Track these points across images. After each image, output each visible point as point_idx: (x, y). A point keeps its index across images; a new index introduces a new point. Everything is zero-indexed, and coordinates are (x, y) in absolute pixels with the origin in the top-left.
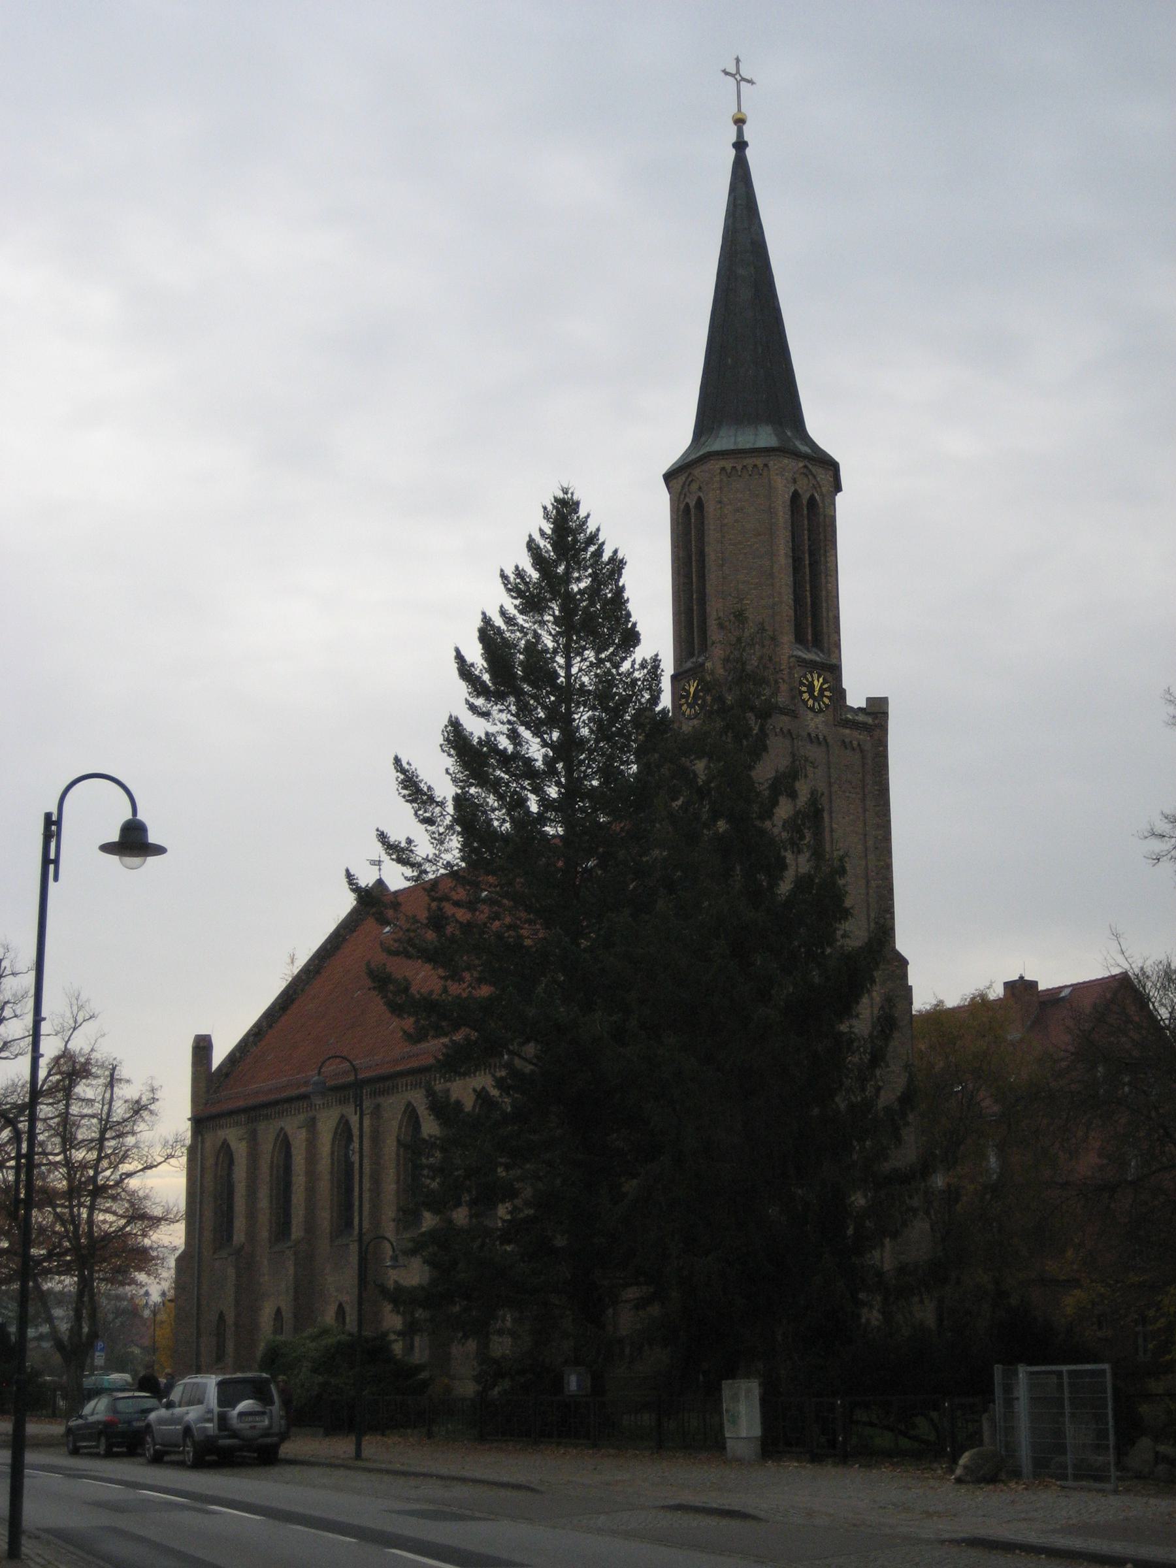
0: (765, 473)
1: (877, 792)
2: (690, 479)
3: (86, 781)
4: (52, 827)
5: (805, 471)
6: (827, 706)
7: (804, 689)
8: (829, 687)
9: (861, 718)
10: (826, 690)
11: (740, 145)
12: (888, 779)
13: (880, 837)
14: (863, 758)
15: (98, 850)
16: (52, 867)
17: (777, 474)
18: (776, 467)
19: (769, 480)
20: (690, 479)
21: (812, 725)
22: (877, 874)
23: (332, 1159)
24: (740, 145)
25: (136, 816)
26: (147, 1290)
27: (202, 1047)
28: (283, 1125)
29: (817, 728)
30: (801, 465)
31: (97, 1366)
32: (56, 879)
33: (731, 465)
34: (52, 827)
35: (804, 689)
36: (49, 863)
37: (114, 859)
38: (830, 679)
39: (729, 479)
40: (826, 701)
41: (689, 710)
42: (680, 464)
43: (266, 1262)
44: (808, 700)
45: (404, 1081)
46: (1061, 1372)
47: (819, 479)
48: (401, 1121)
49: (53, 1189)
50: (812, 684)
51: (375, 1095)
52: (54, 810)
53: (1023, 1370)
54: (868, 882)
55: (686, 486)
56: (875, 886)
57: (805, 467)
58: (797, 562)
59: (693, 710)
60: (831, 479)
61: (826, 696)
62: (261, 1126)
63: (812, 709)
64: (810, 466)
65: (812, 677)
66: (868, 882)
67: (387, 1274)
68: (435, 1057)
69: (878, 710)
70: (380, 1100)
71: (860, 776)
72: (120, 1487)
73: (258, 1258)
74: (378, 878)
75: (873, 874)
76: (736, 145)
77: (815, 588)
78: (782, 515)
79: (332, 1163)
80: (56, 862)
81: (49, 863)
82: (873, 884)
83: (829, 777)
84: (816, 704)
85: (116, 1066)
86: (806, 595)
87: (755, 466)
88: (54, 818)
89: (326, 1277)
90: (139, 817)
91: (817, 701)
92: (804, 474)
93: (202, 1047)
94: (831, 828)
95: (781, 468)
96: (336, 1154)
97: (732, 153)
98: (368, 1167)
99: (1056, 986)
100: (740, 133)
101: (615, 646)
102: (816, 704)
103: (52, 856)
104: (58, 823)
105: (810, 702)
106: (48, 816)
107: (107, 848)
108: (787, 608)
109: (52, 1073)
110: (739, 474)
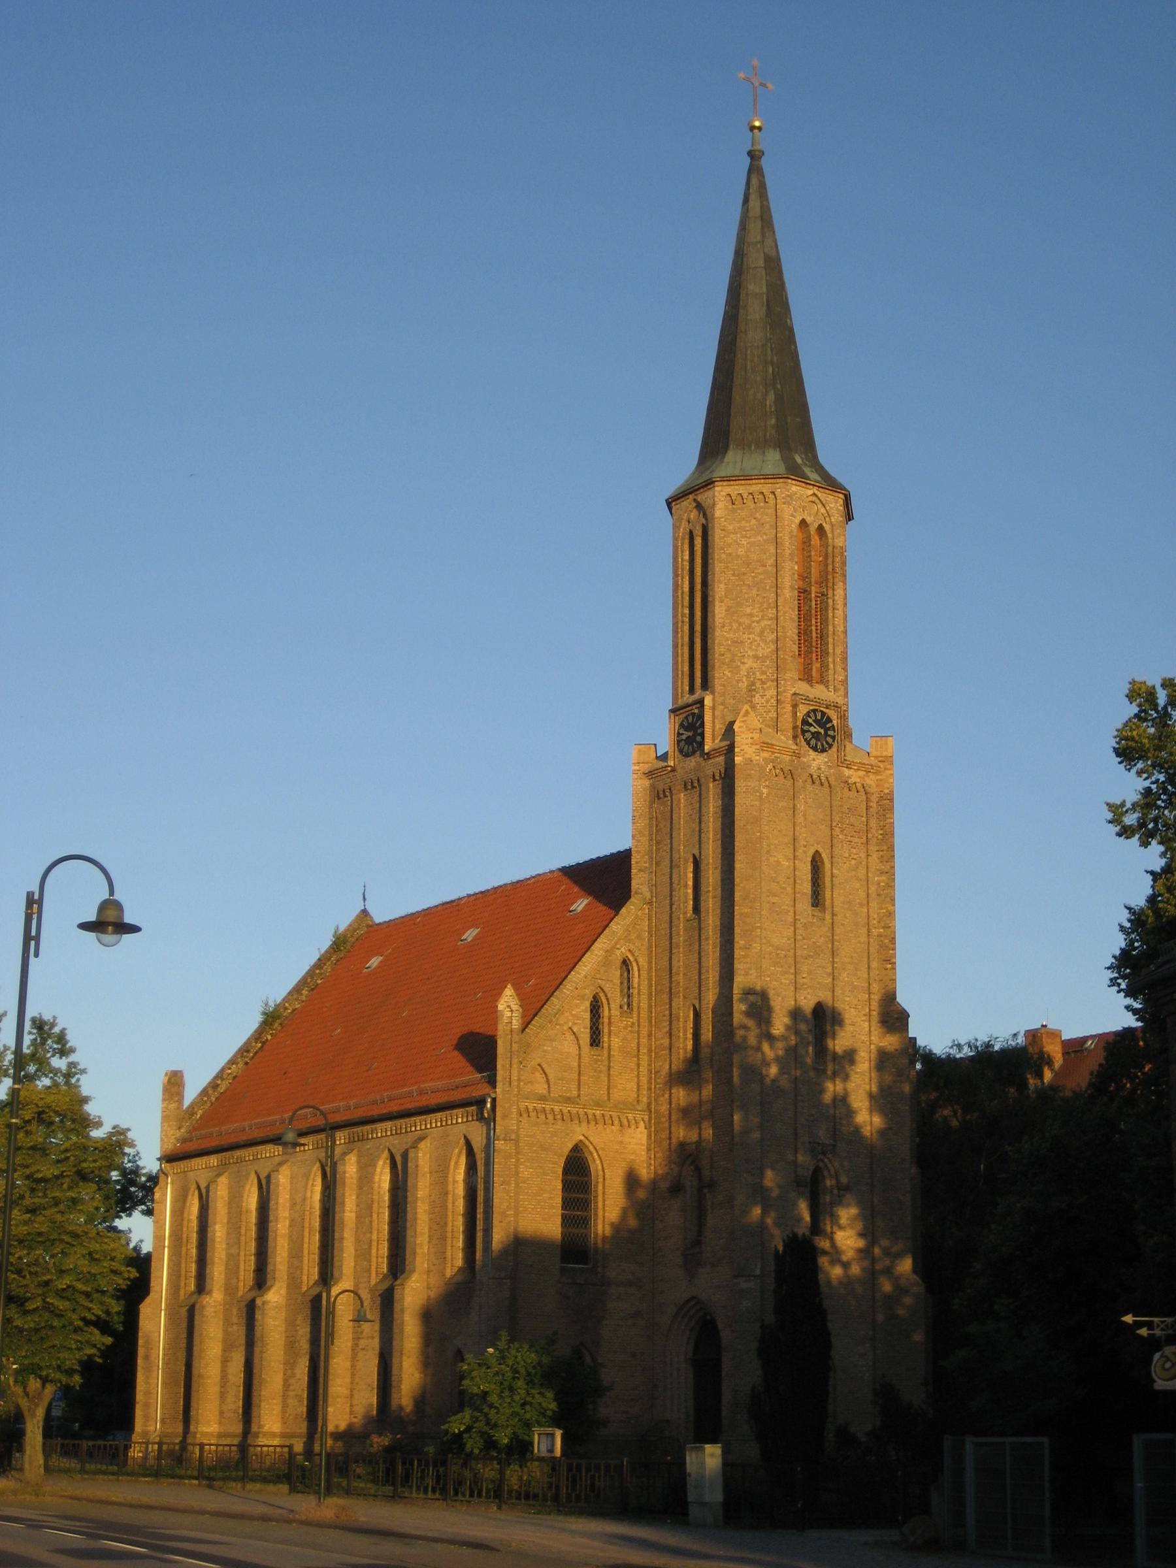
1: (880, 837)
4: (34, 904)
5: (814, 498)
13: (882, 884)
14: (868, 800)
15: (78, 929)
16: (33, 943)
17: (784, 503)
18: (784, 495)
21: (814, 765)
22: (879, 922)
25: (113, 896)
26: (34, 1020)
27: (174, 1083)
29: (819, 769)
30: (810, 492)
31: (1122, 821)
32: (37, 955)
34: (34, 904)
36: (31, 940)
37: (91, 936)
41: (686, 747)
42: (683, 489)
44: (811, 739)
47: (828, 508)
52: (35, 889)
53: (970, 1442)
56: (876, 934)
57: (814, 494)
59: (690, 747)
60: (842, 508)
61: (829, 735)
64: (819, 495)
71: (864, 819)
74: (363, 908)
75: (875, 922)
76: (751, 154)
78: (789, 545)
80: (37, 939)
81: (31, 940)
82: (874, 932)
84: (819, 744)
86: (811, 630)
88: (36, 897)
89: (298, 1328)
90: (117, 896)
91: (819, 740)
92: (813, 502)
93: (174, 1083)
94: (832, 873)
95: (788, 496)
99: (1081, 1035)
102: (819, 744)
103: (33, 933)
104: (40, 902)
106: (30, 896)
107: (85, 926)
108: (791, 643)
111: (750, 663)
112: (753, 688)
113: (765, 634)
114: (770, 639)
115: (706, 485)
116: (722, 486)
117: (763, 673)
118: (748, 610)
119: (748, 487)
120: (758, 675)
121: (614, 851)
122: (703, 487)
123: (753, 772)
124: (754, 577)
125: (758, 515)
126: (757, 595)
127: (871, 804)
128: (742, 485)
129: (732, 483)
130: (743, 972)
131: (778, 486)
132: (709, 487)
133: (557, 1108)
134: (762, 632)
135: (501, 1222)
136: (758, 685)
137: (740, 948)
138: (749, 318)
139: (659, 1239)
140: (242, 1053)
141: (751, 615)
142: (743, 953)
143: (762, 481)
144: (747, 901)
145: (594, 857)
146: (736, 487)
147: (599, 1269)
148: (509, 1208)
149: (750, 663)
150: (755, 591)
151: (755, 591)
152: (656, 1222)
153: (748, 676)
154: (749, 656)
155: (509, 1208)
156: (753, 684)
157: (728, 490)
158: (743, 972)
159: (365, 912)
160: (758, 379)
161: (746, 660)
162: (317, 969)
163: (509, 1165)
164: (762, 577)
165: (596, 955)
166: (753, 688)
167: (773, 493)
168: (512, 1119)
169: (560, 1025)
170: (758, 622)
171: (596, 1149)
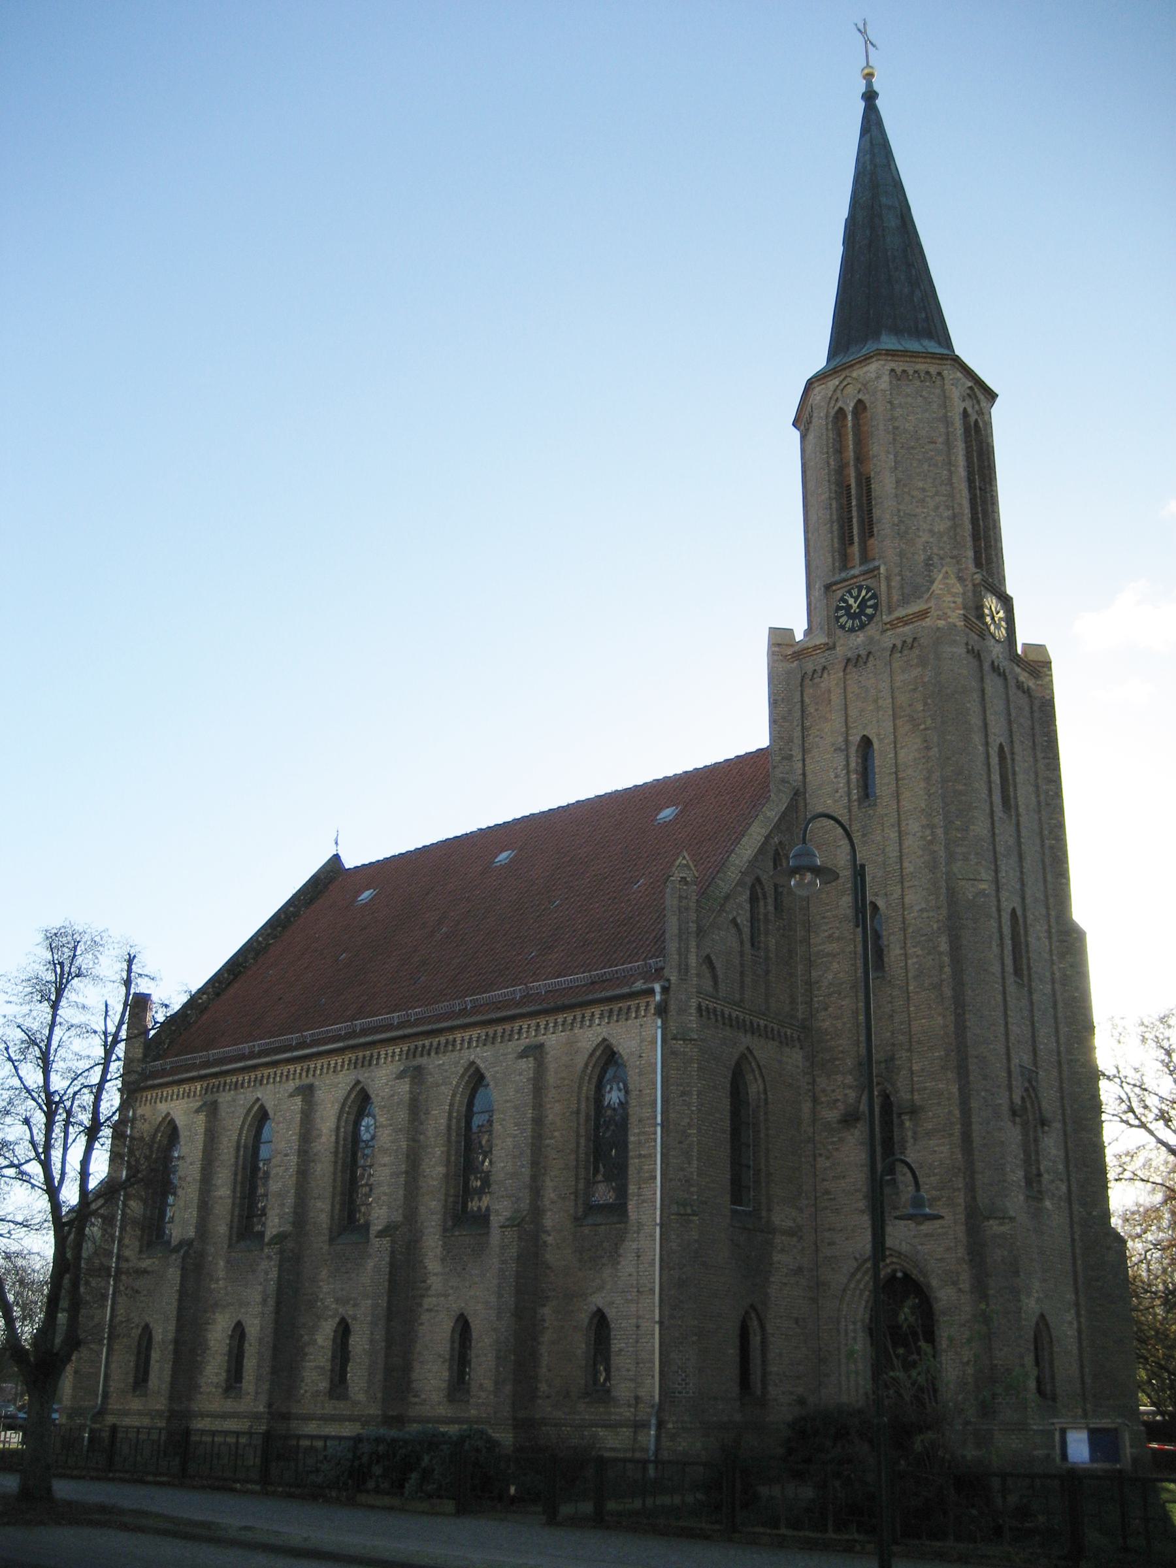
0: (938, 383)
2: (845, 383)
11: (870, 97)
12: (1055, 731)
13: (1051, 793)
17: (952, 385)
18: (951, 377)
19: (944, 391)
20: (845, 383)
23: (337, 1136)
24: (870, 97)
28: (259, 1095)
30: (970, 384)
33: (901, 369)
39: (899, 382)
43: (222, 1263)
45: (467, 1035)
48: (457, 1086)
51: (437, 1053)
54: (1042, 841)
55: (839, 392)
58: (970, 481)
62: (225, 1098)
66: (1042, 841)
67: (424, 1282)
68: (197, 1111)
70: (423, 1061)
73: (210, 1259)
77: (986, 513)
79: (337, 1142)
83: (1010, 715)
85: (135, 956)
87: (928, 373)
89: (321, 1284)
96: (342, 1130)
97: (861, 105)
98: (405, 1143)
100: (869, 84)
110: (911, 377)
111: (925, 537)
112: (931, 562)
113: (940, 510)
114: (946, 514)
115: (866, 359)
116: (886, 360)
117: (942, 548)
118: (920, 484)
119: (913, 364)
120: (935, 550)
121: (690, 768)
122: (860, 362)
123: (958, 638)
124: (924, 453)
125: (924, 393)
126: (929, 471)
127: (247, 1051)
128: (907, 362)
129: (896, 358)
130: (961, 857)
131: (944, 367)
132: (868, 362)
133: (727, 1012)
134: (937, 508)
135: (680, 1142)
136: (936, 559)
137: (957, 829)
138: (885, 225)
139: (824, 1180)
140: (214, 984)
141: (924, 490)
142: (959, 835)
143: (928, 360)
144: (960, 777)
145: (660, 777)
146: (901, 363)
147: (764, 1214)
148: (690, 1126)
149: (925, 537)
150: (926, 466)
151: (926, 466)
152: (819, 1159)
153: (925, 550)
154: (924, 530)
155: (690, 1126)
156: (930, 558)
157: (893, 365)
158: (961, 857)
159: (336, 858)
160: (902, 277)
161: (921, 534)
162: (291, 906)
163: (690, 1071)
164: (933, 453)
165: (756, 840)
166: (931, 562)
167: (939, 374)
168: (690, 1015)
169: (726, 912)
170: (932, 497)
171: (759, 1066)
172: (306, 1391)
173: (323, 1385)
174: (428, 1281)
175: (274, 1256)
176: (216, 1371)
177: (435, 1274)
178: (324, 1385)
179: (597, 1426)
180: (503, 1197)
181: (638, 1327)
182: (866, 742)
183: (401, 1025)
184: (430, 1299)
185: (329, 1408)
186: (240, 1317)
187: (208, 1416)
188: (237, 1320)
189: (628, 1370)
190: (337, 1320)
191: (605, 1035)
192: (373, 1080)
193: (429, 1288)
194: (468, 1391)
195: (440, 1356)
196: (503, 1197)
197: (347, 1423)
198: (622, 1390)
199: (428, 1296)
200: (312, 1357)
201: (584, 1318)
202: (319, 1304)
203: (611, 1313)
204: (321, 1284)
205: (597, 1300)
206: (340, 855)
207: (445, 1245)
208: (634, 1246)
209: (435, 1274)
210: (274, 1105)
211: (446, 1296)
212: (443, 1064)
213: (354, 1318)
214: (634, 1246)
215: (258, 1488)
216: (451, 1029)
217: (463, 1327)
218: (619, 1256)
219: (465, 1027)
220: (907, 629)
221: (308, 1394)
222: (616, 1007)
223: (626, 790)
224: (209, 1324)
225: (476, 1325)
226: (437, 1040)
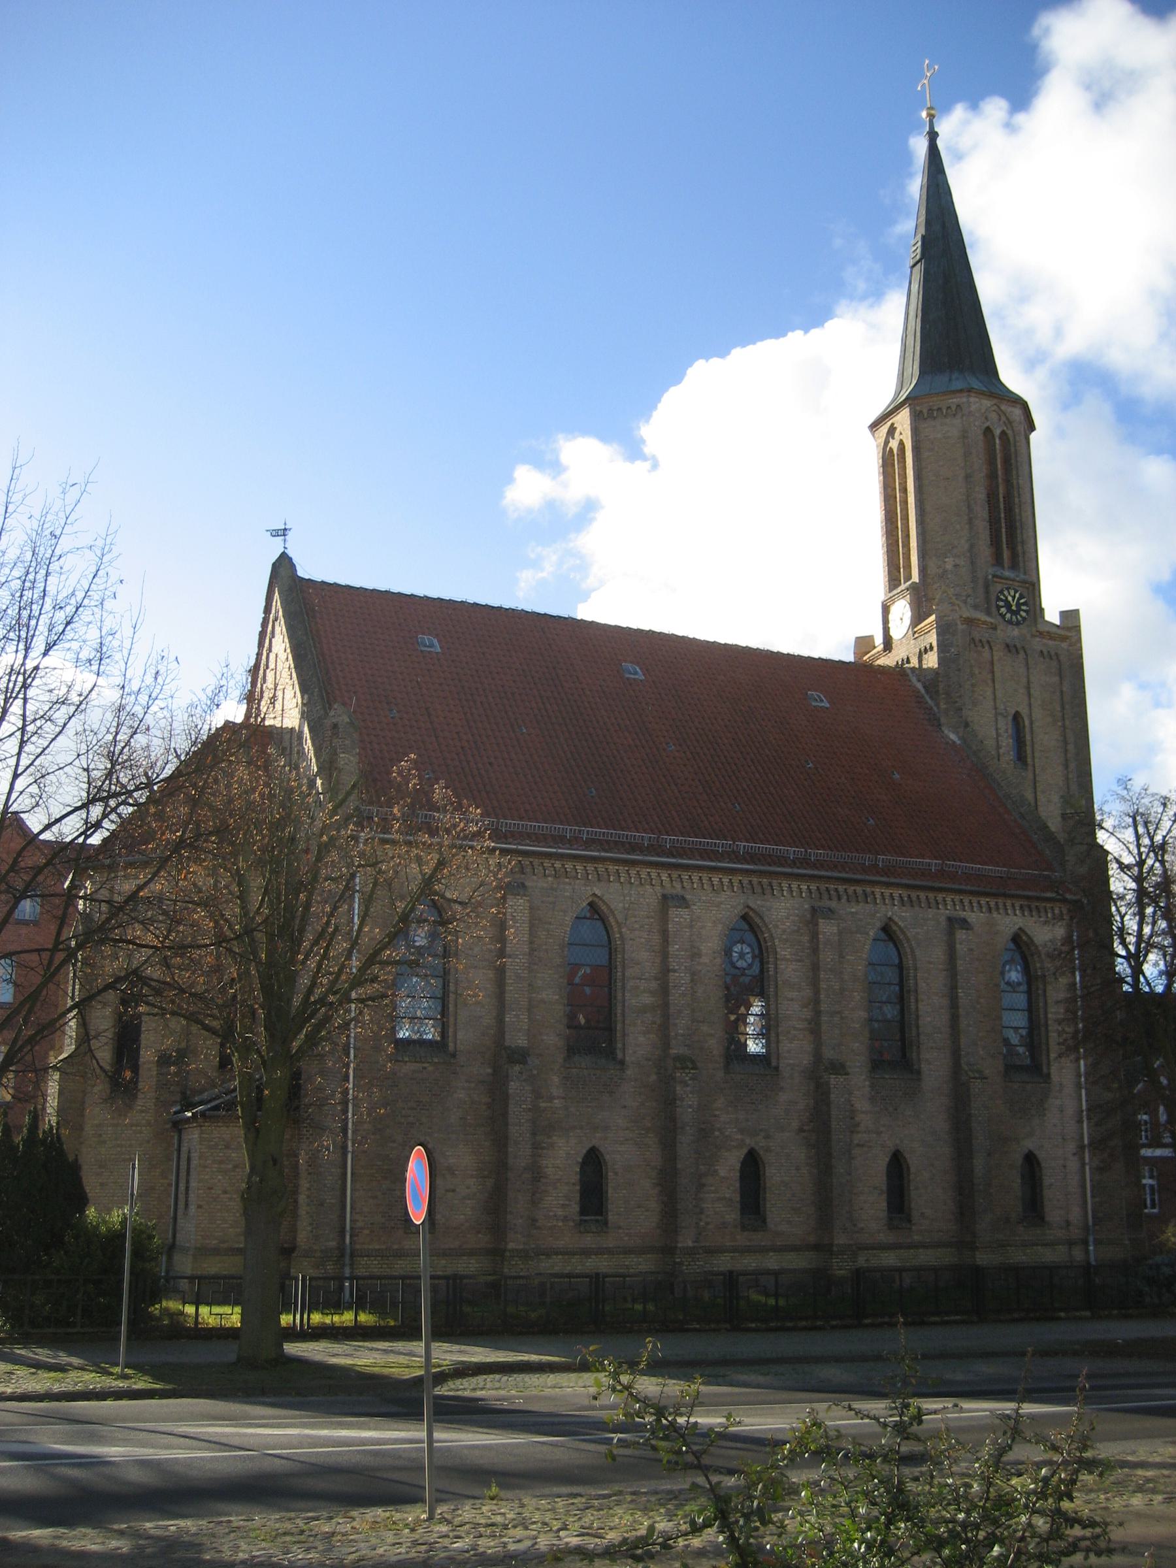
3: (264, 604)
6: (1024, 619)
7: (1001, 604)
8: (1020, 595)
9: (1060, 632)
10: (1023, 604)
35: (1001, 604)
38: (1025, 594)
40: (1024, 614)
46: (82, 1327)
49: (507, 1076)
50: (1006, 600)
63: (1010, 622)
65: (1004, 595)
69: (1071, 618)
72: (16, 1463)
84: (1014, 617)
101: (1037, 1540)
105: (1008, 615)
109: (19, 772)
172: (707, 1224)
173: (733, 1216)
174: (857, 1119)
175: (690, 1082)
176: (561, 1202)
177: (863, 1112)
178: (732, 1216)
179: (1037, 1245)
180: (932, 1048)
181: (1065, 1167)
182: (1017, 717)
183: (794, 864)
184: (860, 1135)
185: (742, 1239)
186: (595, 1142)
187: (557, 1254)
188: (590, 1146)
189: (1058, 1200)
190: (745, 1151)
191: (1021, 925)
192: (769, 910)
193: (858, 1125)
194: (910, 1221)
195: (875, 1188)
196: (932, 1048)
197: (771, 1254)
198: (1054, 1215)
199: (858, 1132)
200: (713, 1188)
201: (1018, 1159)
202: (717, 1133)
203: (1041, 1155)
204: (717, 1113)
205: (1029, 1144)
206: (291, 555)
207: (872, 1086)
208: (1058, 1102)
209: (863, 1112)
210: (624, 908)
211: (879, 1133)
212: (856, 913)
213: (768, 1150)
214: (1058, 1102)
215: (1088, 1314)
216: (873, 883)
217: (897, 1165)
218: (1044, 1109)
219: (888, 885)
220: (1051, 643)
221: (710, 1227)
222: (1034, 904)
223: (639, 632)
224: (543, 1148)
225: (914, 1161)
226: (853, 888)
